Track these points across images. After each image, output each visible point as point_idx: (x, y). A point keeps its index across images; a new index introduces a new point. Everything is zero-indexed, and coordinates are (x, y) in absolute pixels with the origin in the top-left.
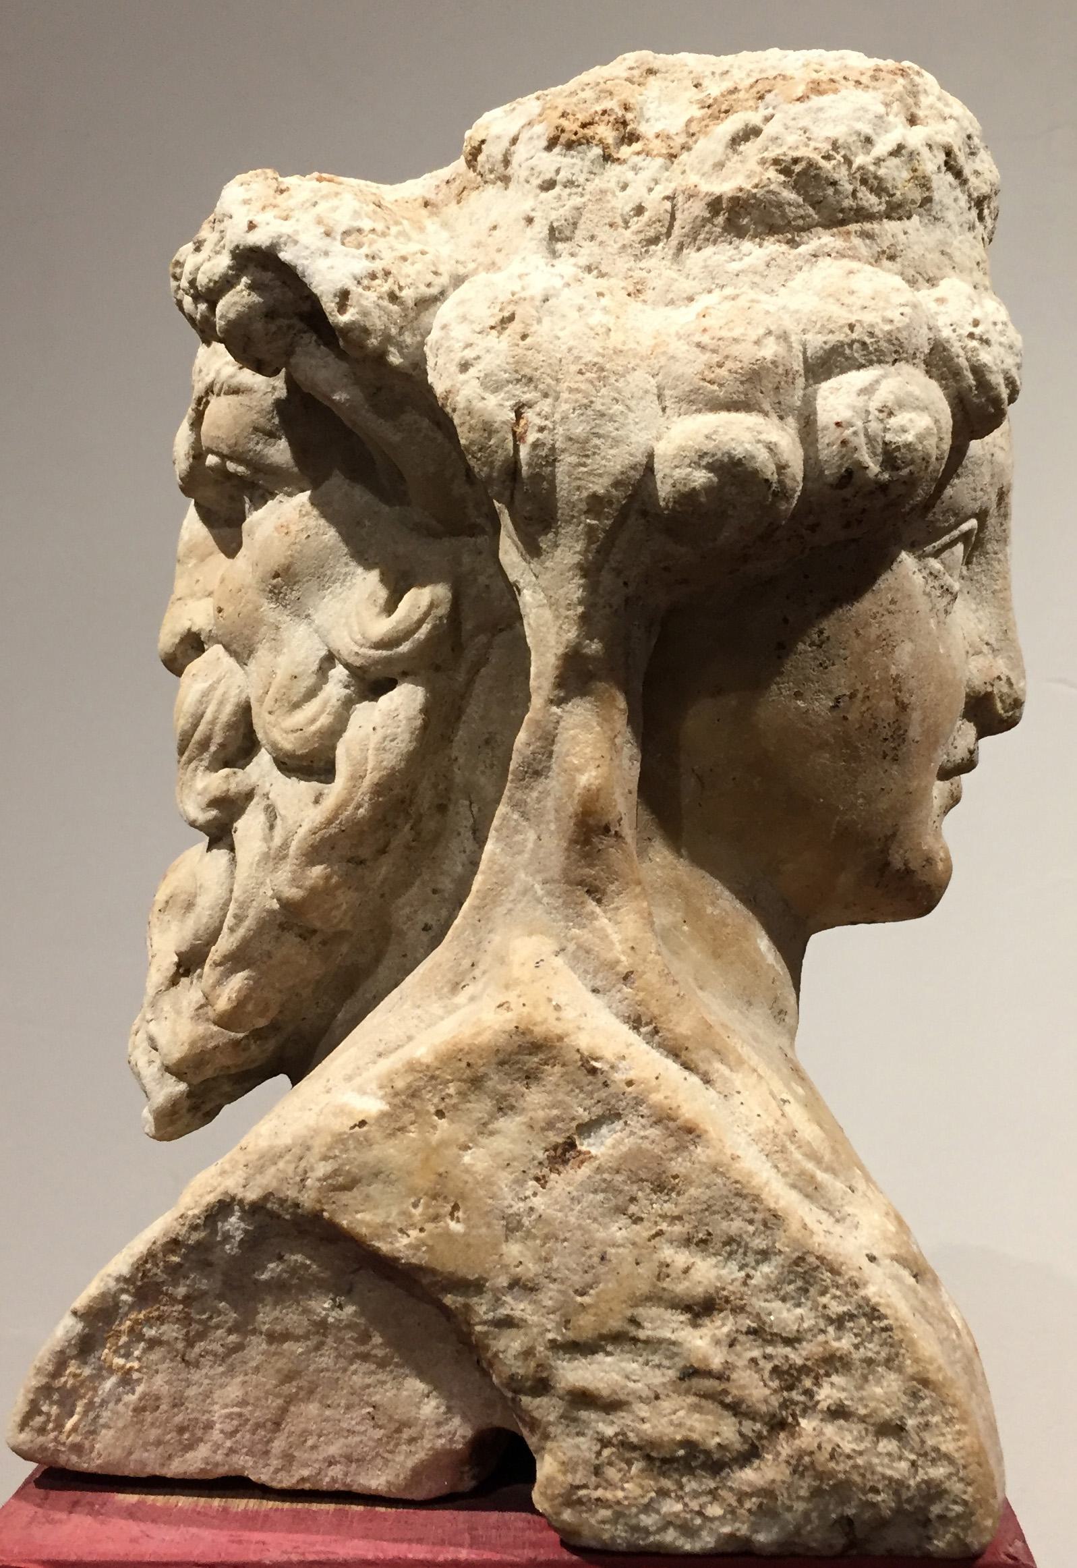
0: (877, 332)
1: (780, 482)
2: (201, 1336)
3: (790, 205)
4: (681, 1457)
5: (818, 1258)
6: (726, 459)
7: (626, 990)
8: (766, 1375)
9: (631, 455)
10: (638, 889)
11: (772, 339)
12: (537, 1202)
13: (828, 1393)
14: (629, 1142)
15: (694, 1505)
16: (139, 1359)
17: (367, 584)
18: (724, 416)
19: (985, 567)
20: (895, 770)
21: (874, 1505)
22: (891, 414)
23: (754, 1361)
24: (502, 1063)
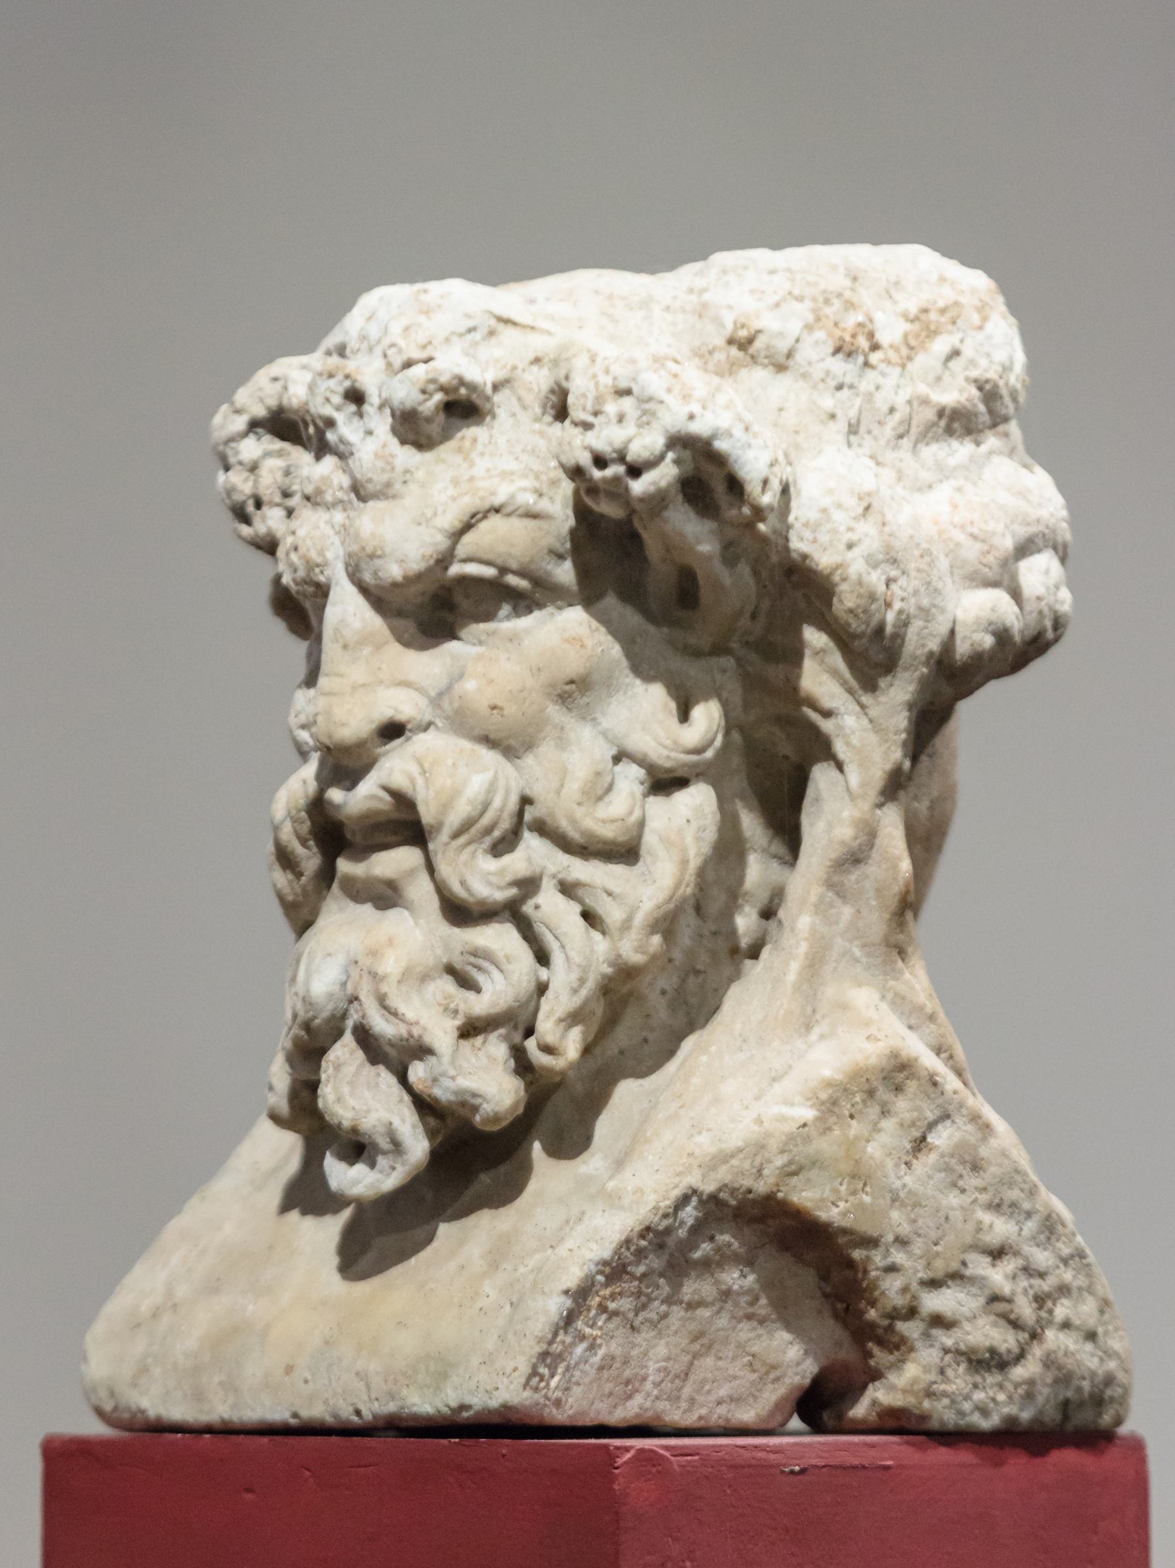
2: (644, 1307)
7: (932, 1026)
12: (908, 1180)
13: (1061, 1311)
14: (958, 1135)
15: (991, 1393)
16: (601, 1328)
17: (653, 698)
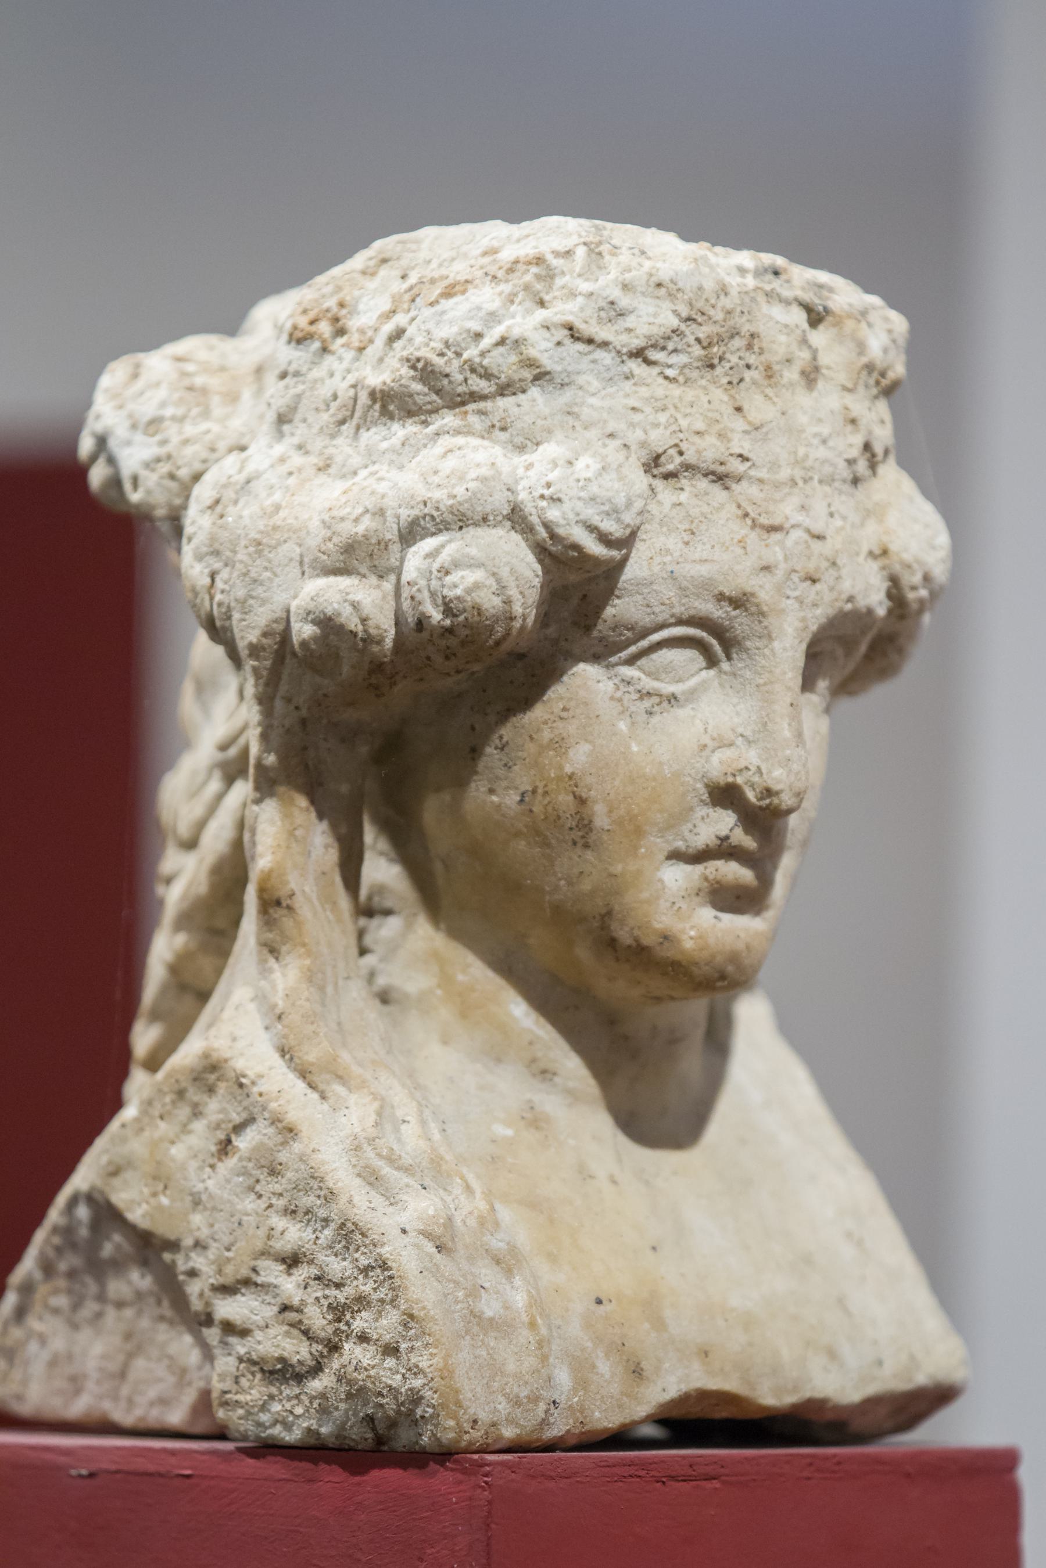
0: (442, 507)
1: (365, 631)
3: (418, 394)
4: (279, 1370)
5: (353, 1223)
6: (322, 616)
8: (325, 1309)
9: (273, 611)
10: (303, 950)
11: (368, 516)
12: (210, 1183)
13: (359, 1324)
14: (258, 1137)
15: (288, 1406)
18: (332, 580)
19: (748, 662)
20: (589, 855)
21: (381, 1406)
22: (447, 573)
23: (317, 1299)
24: (195, 1079)
